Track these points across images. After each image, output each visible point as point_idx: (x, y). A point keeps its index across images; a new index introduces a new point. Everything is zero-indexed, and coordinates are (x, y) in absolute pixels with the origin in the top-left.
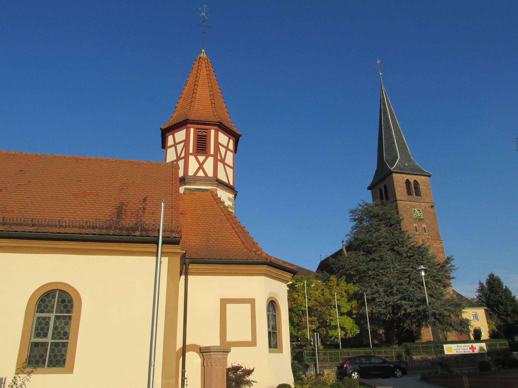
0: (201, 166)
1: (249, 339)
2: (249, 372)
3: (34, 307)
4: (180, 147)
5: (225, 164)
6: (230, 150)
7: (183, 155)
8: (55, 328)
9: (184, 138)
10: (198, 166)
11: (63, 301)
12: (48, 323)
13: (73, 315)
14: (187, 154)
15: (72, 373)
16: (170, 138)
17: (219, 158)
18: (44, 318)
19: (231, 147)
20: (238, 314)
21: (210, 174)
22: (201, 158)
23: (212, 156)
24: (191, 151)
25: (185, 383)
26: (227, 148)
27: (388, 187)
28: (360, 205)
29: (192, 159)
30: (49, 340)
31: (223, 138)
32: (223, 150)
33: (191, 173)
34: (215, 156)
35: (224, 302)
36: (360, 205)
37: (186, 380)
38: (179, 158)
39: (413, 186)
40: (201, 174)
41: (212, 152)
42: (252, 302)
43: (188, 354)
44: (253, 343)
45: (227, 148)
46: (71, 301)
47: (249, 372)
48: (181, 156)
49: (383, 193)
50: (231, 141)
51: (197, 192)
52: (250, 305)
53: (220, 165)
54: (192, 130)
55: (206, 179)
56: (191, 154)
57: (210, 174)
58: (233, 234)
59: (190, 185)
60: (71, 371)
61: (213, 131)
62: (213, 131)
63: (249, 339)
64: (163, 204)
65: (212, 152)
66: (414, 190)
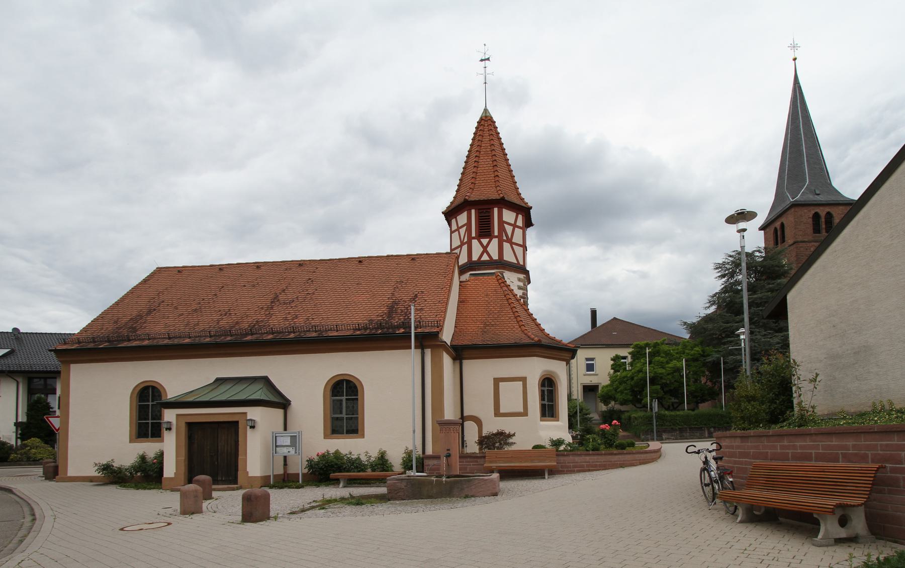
2: (510, 436)
3: (329, 393)
4: (463, 231)
5: (512, 243)
7: (466, 240)
9: (465, 221)
11: (350, 387)
12: (341, 404)
13: (359, 397)
14: (470, 238)
16: (454, 221)
17: (505, 238)
18: (338, 400)
19: (520, 223)
21: (495, 257)
22: (485, 241)
23: (496, 237)
24: (474, 235)
26: (515, 226)
27: (786, 225)
28: (730, 256)
29: (475, 243)
30: (344, 415)
31: (509, 216)
32: (509, 229)
33: (475, 258)
35: (497, 381)
36: (730, 256)
38: (462, 244)
39: (823, 220)
40: (485, 258)
41: (496, 233)
42: (524, 380)
43: (467, 424)
44: (525, 413)
45: (515, 226)
46: (355, 387)
47: (510, 436)
49: (779, 233)
50: (520, 217)
53: (506, 246)
54: (473, 211)
55: (491, 264)
56: (474, 238)
57: (495, 257)
60: (363, 436)
61: (496, 210)
62: (496, 210)
65: (496, 233)
66: (824, 226)
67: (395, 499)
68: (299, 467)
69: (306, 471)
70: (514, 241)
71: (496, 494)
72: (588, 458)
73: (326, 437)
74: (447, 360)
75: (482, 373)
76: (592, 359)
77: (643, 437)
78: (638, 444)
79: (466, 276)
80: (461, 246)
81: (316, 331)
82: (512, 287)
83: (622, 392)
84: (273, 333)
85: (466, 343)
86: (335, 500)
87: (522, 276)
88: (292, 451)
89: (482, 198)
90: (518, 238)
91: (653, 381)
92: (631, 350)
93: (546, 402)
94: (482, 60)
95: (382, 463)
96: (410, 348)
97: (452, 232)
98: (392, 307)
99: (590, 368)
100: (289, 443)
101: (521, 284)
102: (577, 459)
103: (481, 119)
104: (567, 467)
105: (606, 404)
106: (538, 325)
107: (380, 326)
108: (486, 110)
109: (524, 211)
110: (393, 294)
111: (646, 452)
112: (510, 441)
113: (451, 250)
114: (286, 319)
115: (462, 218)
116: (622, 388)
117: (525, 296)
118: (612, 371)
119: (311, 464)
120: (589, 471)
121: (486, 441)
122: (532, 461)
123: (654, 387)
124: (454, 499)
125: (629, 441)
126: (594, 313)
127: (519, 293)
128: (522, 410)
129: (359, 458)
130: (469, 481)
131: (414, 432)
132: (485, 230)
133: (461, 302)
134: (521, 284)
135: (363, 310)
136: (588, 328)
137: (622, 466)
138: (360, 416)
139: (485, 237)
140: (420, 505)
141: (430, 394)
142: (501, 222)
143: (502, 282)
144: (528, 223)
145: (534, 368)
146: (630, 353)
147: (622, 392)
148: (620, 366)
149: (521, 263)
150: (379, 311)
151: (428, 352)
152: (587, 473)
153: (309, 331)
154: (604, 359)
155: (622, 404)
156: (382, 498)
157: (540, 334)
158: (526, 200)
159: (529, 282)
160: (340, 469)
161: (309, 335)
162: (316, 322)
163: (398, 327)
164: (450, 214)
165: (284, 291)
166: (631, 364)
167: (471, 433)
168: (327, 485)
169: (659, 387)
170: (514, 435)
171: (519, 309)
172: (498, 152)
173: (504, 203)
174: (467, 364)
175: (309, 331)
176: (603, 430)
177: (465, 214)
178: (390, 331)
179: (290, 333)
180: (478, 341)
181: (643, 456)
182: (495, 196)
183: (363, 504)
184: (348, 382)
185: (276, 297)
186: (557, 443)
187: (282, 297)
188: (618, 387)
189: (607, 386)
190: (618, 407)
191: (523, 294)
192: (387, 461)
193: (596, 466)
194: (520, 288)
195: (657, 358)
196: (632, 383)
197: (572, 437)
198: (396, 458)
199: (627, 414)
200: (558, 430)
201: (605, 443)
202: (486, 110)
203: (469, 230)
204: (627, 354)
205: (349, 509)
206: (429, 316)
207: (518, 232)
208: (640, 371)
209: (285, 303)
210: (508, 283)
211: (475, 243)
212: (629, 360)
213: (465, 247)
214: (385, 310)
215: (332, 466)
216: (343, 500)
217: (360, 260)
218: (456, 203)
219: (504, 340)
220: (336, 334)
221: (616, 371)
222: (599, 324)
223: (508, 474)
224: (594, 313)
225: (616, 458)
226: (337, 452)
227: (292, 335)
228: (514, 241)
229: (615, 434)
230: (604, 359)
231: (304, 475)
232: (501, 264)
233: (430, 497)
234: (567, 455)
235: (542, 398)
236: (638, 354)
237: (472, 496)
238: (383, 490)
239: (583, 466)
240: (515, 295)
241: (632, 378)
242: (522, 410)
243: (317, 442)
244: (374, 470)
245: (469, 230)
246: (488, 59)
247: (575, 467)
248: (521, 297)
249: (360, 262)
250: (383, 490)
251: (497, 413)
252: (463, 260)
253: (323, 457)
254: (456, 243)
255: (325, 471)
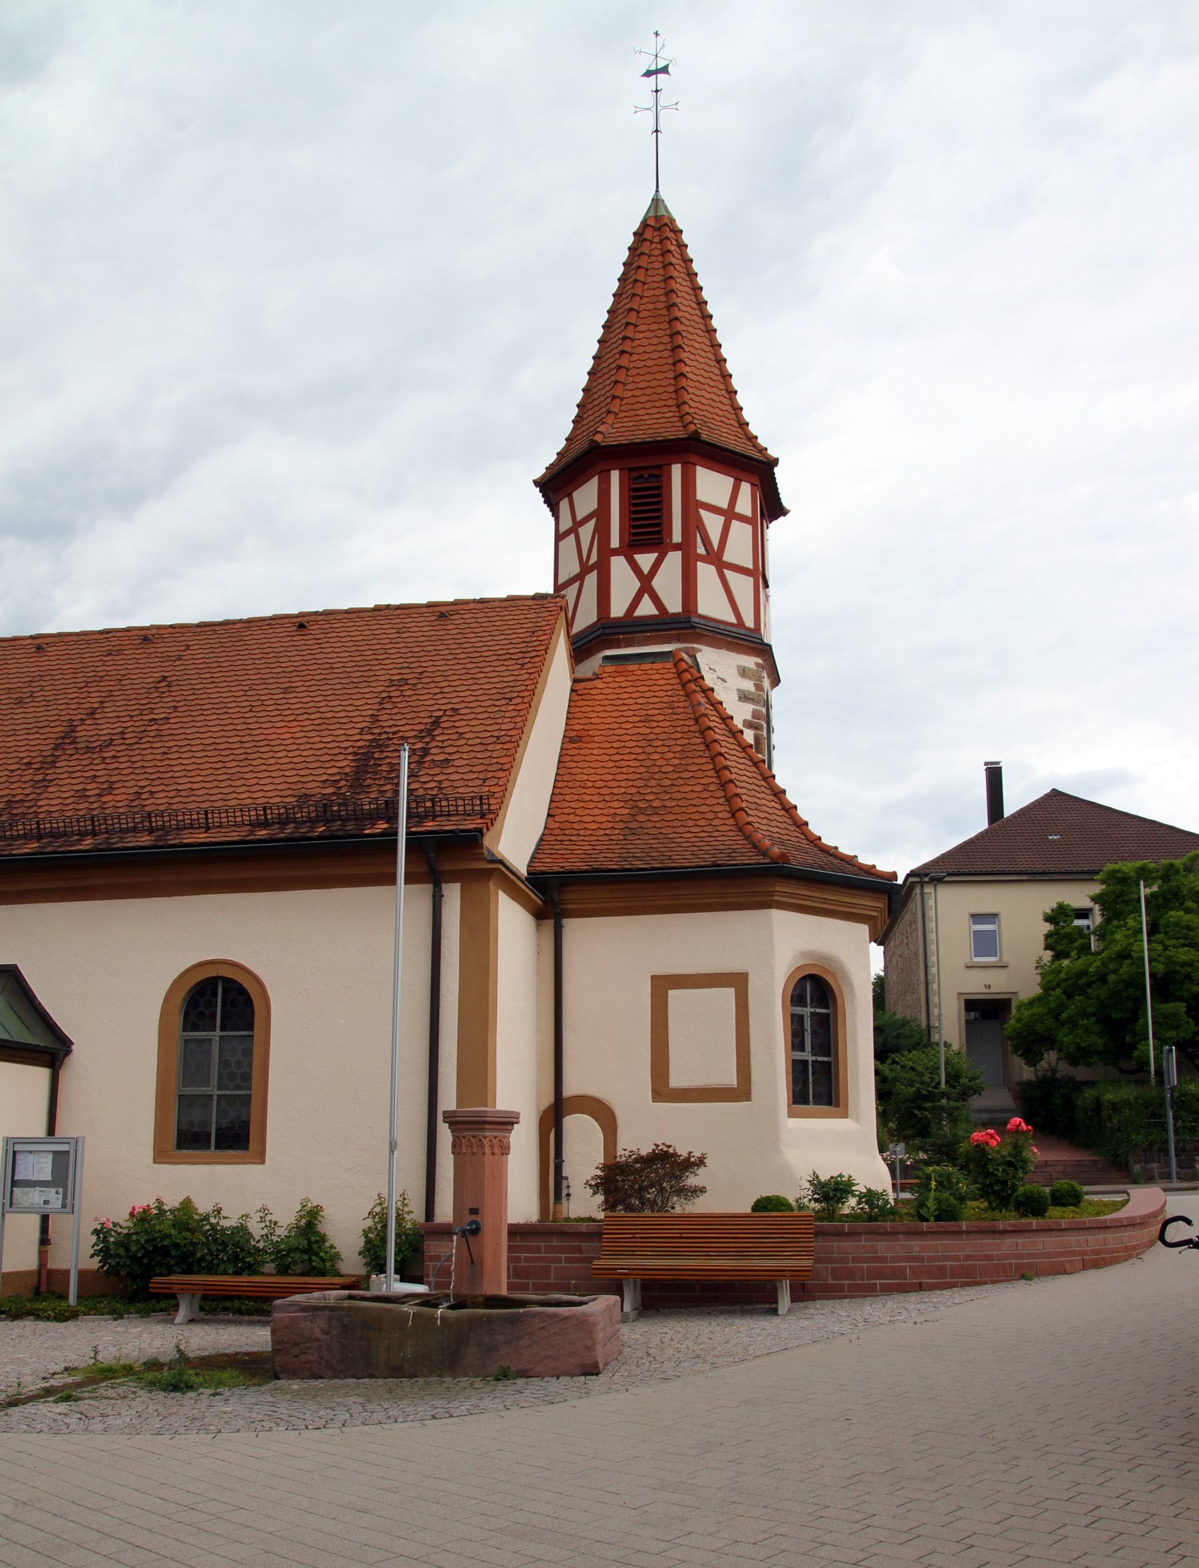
0: (646, 582)
1: (730, 1079)
2: (690, 1164)
3: (178, 1020)
4: (586, 531)
5: (722, 568)
6: (742, 518)
7: (594, 559)
8: (224, 1064)
9: (593, 505)
10: (656, 583)
14: (606, 553)
15: (263, 1162)
16: (564, 505)
17: (701, 550)
19: (744, 506)
20: (701, 1022)
21: (674, 605)
22: (645, 560)
23: (676, 547)
24: (615, 542)
25: (564, 1192)
29: (619, 565)
31: (712, 486)
32: (713, 524)
33: (618, 610)
34: (686, 547)
35: (662, 985)
37: (565, 1183)
38: (585, 569)
40: (646, 608)
41: (677, 537)
42: (738, 981)
44: (741, 1092)
45: (730, 514)
48: (591, 562)
50: (746, 488)
51: (635, 667)
52: (672, 993)
53: (706, 573)
54: (615, 476)
56: (616, 552)
57: (674, 605)
58: (712, 788)
59: (619, 647)
60: (261, 1158)
61: (676, 470)
63: (730, 1079)
64: (405, 755)
65: (677, 537)
67: (294, 1374)
68: (76, 1254)
69: (95, 1264)
70: (727, 557)
71: (592, 1370)
72: (916, 1245)
73: (161, 1156)
74: (512, 922)
75: (617, 953)
76: (992, 917)
77: (1137, 1168)
78: (1096, 1195)
79: (594, 664)
80: (580, 578)
81: (151, 831)
82: (719, 695)
83: (1073, 1023)
84: (39, 837)
85: (575, 864)
86: (128, 1370)
87: (750, 661)
88: (54, 1197)
89: (640, 436)
90: (738, 549)
91: (1164, 987)
92: (1097, 889)
93: (807, 1056)
94: (648, 74)
95: (307, 1248)
96: (391, 880)
97: (559, 537)
98: (369, 755)
99: (985, 943)
100: (47, 1175)
101: (749, 686)
102: (883, 1247)
103: (645, 225)
104: (851, 1274)
105: (1032, 1057)
106: (790, 809)
107: (325, 813)
108: (657, 202)
109: (756, 469)
110: (375, 718)
111: (1120, 1225)
112: (691, 1181)
113: (558, 588)
114: (83, 795)
115: (586, 497)
116: (1071, 1010)
117: (762, 721)
118: (1048, 955)
119: (108, 1243)
120: (920, 1288)
121: (625, 1180)
122: (741, 1255)
123: (1168, 1007)
124: (465, 1381)
125: (1063, 1184)
126: (994, 776)
127: (740, 713)
128: (732, 1080)
129: (242, 1230)
130: (513, 1321)
131: (393, 1147)
132: (646, 529)
133: (573, 739)
134: (749, 686)
135: (281, 768)
136: (980, 823)
137: (1024, 1272)
138: (255, 1093)
139: (645, 548)
140: (350, 1396)
141: (457, 1021)
142: (691, 504)
143: (690, 680)
144: (772, 507)
145: (786, 939)
146: (1095, 899)
147: (1073, 1023)
148: (1069, 937)
149: (749, 622)
150: (287, 767)
151: (453, 894)
152: (913, 1297)
153: (135, 829)
154: (1023, 914)
155: (1073, 1061)
156: (252, 1369)
157: (793, 834)
158: (762, 441)
159: (776, 681)
160: (188, 1262)
161: (131, 841)
162: (157, 803)
163: (373, 817)
164: (555, 486)
165: (92, 713)
166: (1102, 933)
167: (584, 1150)
168: (145, 1314)
169: (1181, 1007)
170: (701, 1162)
171: (736, 764)
172: (685, 308)
173: (698, 450)
174: (574, 928)
175: (135, 829)
176: (980, 1149)
177: (593, 485)
178: (351, 827)
179: (83, 834)
180: (609, 860)
181: (1093, 1240)
182: (674, 431)
183: (190, 1387)
184: (227, 981)
185: (69, 736)
186: (833, 1191)
187: (82, 733)
188: (1061, 1007)
189: (1032, 1003)
190: (1064, 1069)
191: (755, 714)
192: (323, 1239)
193: (942, 1271)
194: (744, 697)
195: (1175, 915)
196: (1103, 992)
197: (891, 1167)
198: (345, 1234)
199: (1089, 1094)
200: (847, 1147)
201: (985, 1193)
202: (657, 202)
203: (602, 531)
204: (1086, 903)
205: (148, 1403)
206: (460, 781)
207: (741, 533)
208: (1124, 955)
209: (89, 749)
210: (709, 681)
211: (619, 565)
212: (1097, 918)
213: (592, 579)
214: (346, 764)
215: (165, 1251)
216: (103, 1375)
217: (302, 623)
218: (572, 455)
219: (682, 858)
220: (201, 837)
221: (1058, 956)
222: (1009, 809)
223: (666, 1296)
224: (994, 776)
225: (1007, 1245)
226: (187, 1204)
227: (88, 843)
228: (727, 557)
229: (1016, 1163)
230: (1023, 914)
231: (82, 1274)
232: (687, 625)
233: (396, 1372)
234: (853, 1234)
235: (796, 1040)
236: (1116, 903)
237: (524, 1374)
238: (254, 1338)
239: (899, 1273)
240: (727, 719)
241: (1103, 979)
242: (732, 1080)
243: (129, 1172)
244: (283, 1270)
245: (602, 531)
246: (665, 70)
247: (881, 1274)
248: (749, 725)
249: (302, 626)
250: (254, 1338)
251: (662, 1091)
252: (586, 616)
253: (142, 1218)
254: (571, 567)
255: (152, 1265)
